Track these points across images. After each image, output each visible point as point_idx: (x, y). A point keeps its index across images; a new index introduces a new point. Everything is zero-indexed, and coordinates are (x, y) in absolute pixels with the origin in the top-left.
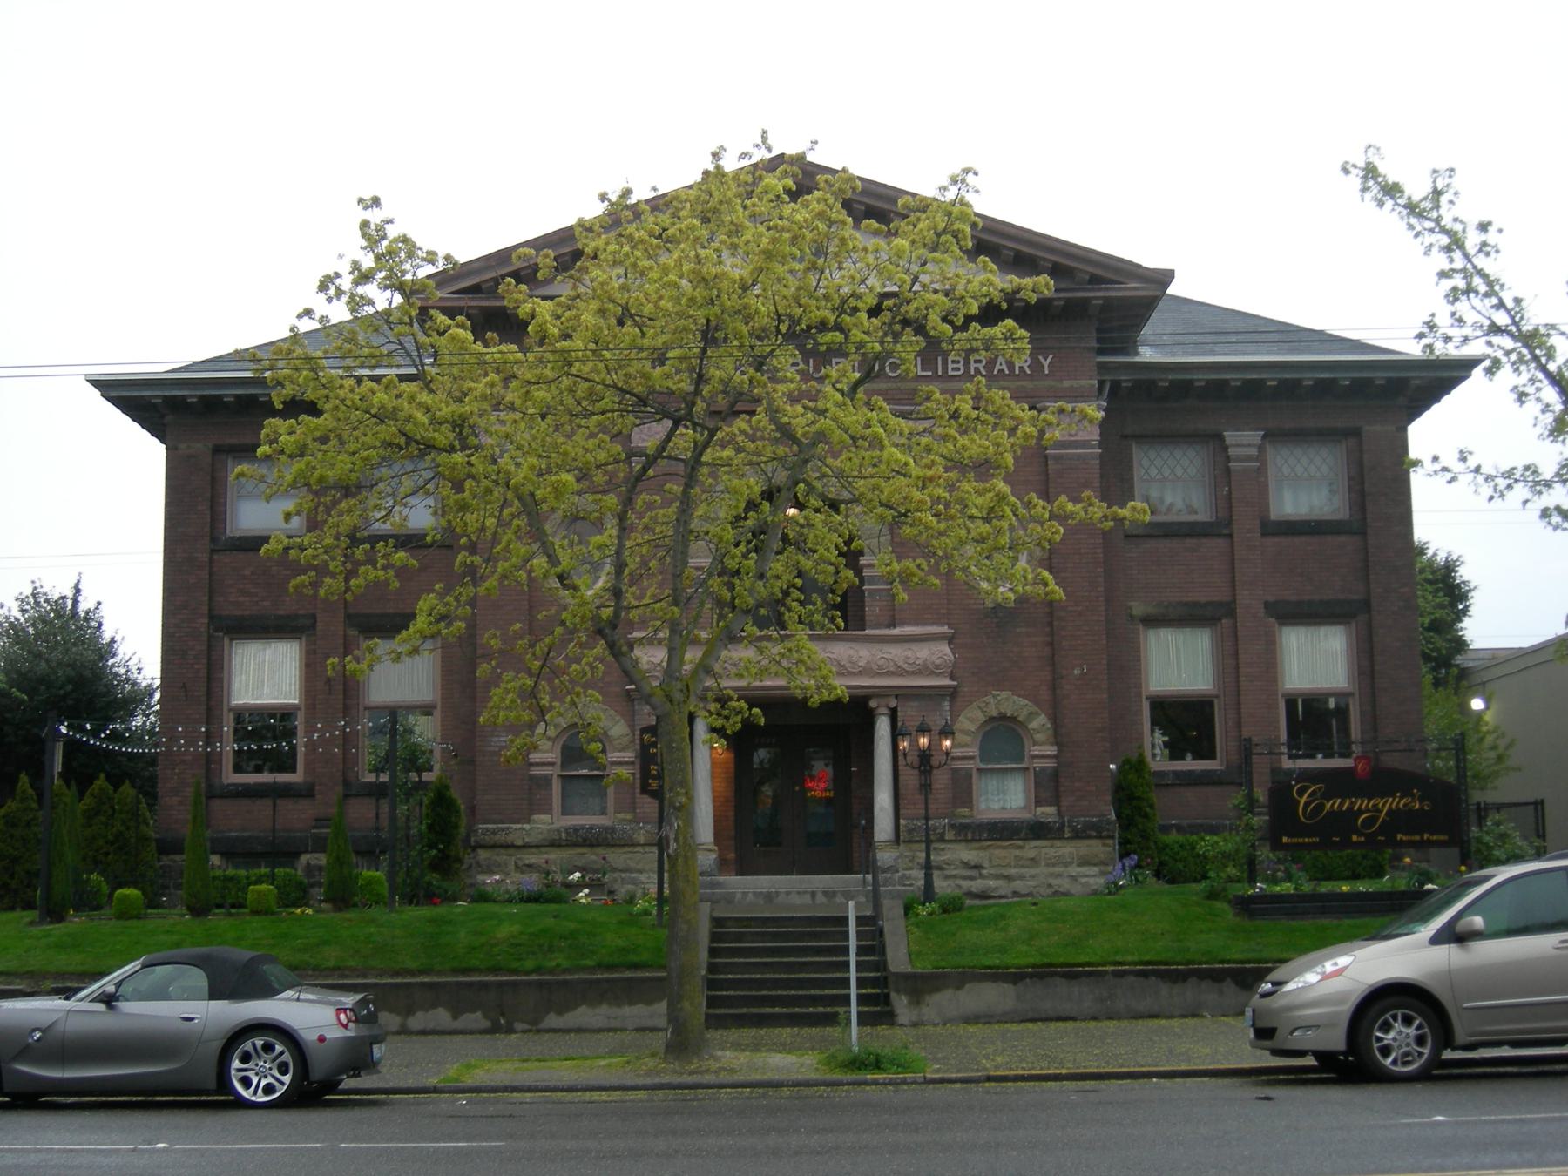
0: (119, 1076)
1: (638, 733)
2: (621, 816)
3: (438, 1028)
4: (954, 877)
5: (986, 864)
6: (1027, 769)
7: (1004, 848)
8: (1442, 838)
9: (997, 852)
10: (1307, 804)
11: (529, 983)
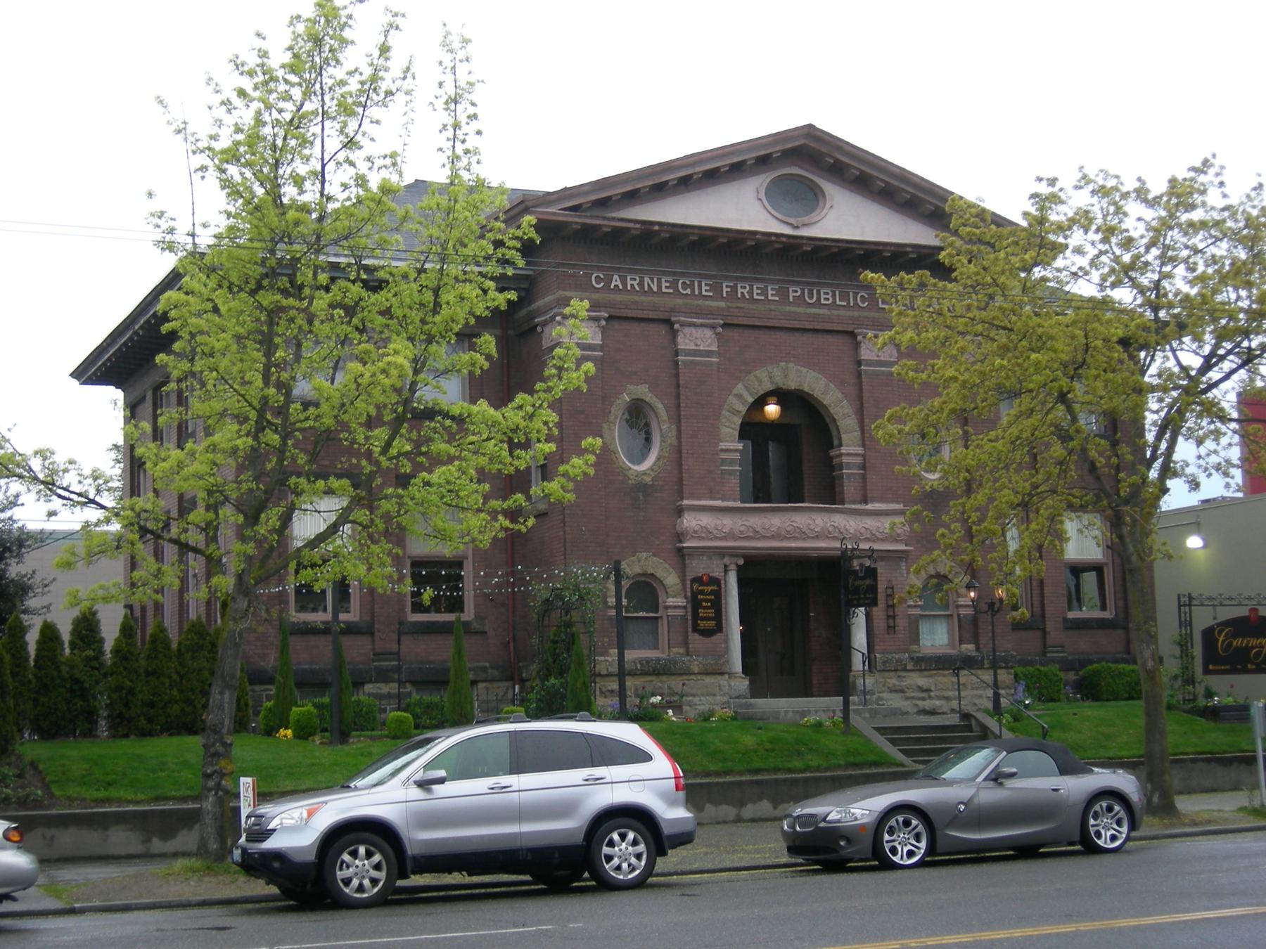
0: (989, 839)
1: (689, 582)
2: (675, 650)
3: (763, 817)
4: (912, 698)
5: (933, 689)
6: (951, 616)
7: (944, 676)
8: (1227, 667)
9: (940, 678)
10: (1223, 641)
11: (826, 778)
